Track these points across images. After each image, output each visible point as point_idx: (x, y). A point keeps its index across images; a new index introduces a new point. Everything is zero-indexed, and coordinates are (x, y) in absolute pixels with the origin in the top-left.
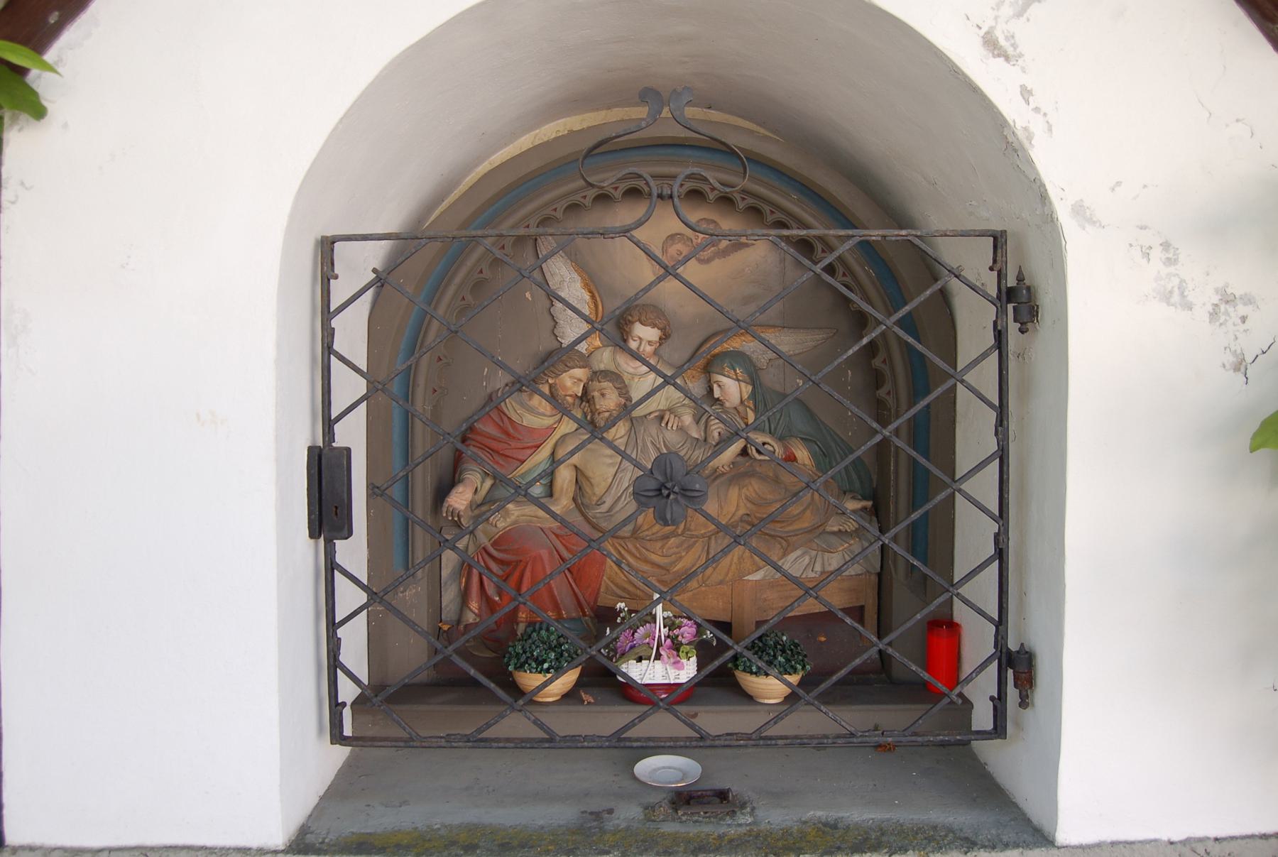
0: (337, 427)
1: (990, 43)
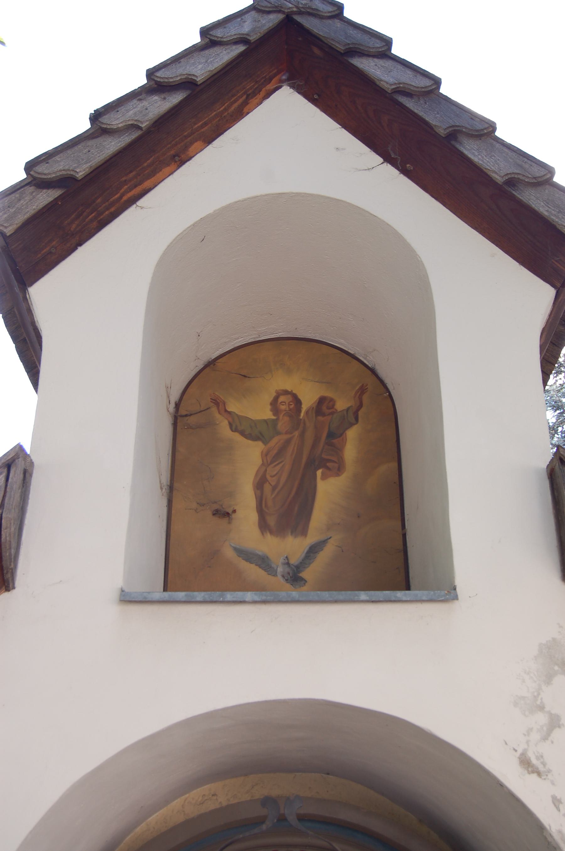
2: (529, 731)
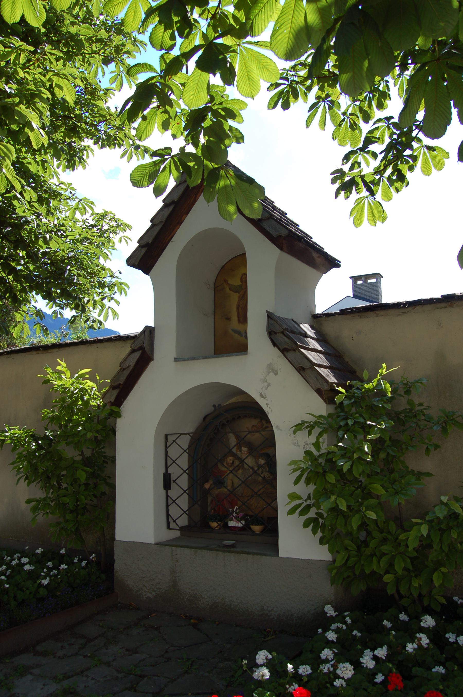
0: (168, 469)
1: (261, 395)
2: (263, 387)
